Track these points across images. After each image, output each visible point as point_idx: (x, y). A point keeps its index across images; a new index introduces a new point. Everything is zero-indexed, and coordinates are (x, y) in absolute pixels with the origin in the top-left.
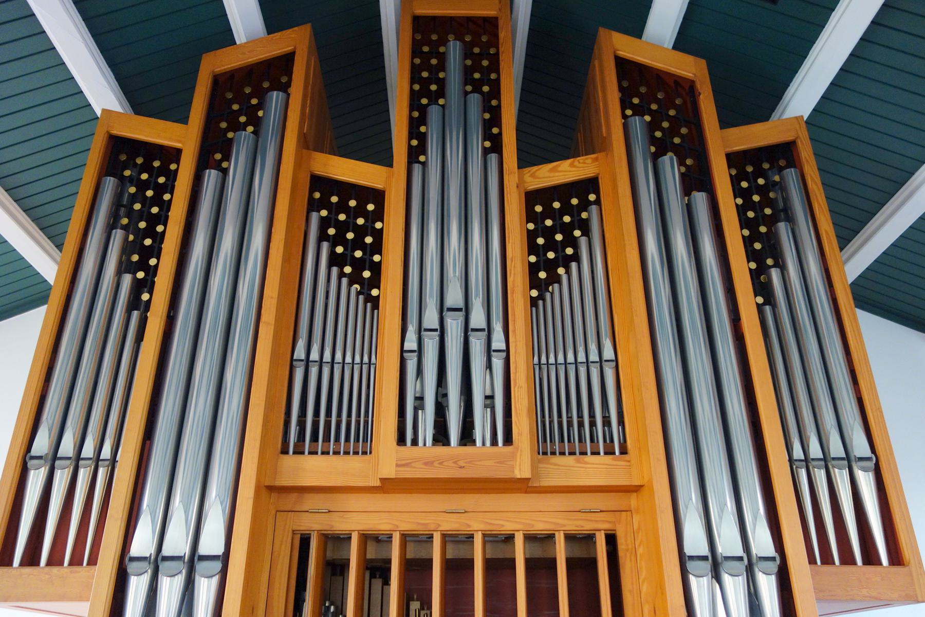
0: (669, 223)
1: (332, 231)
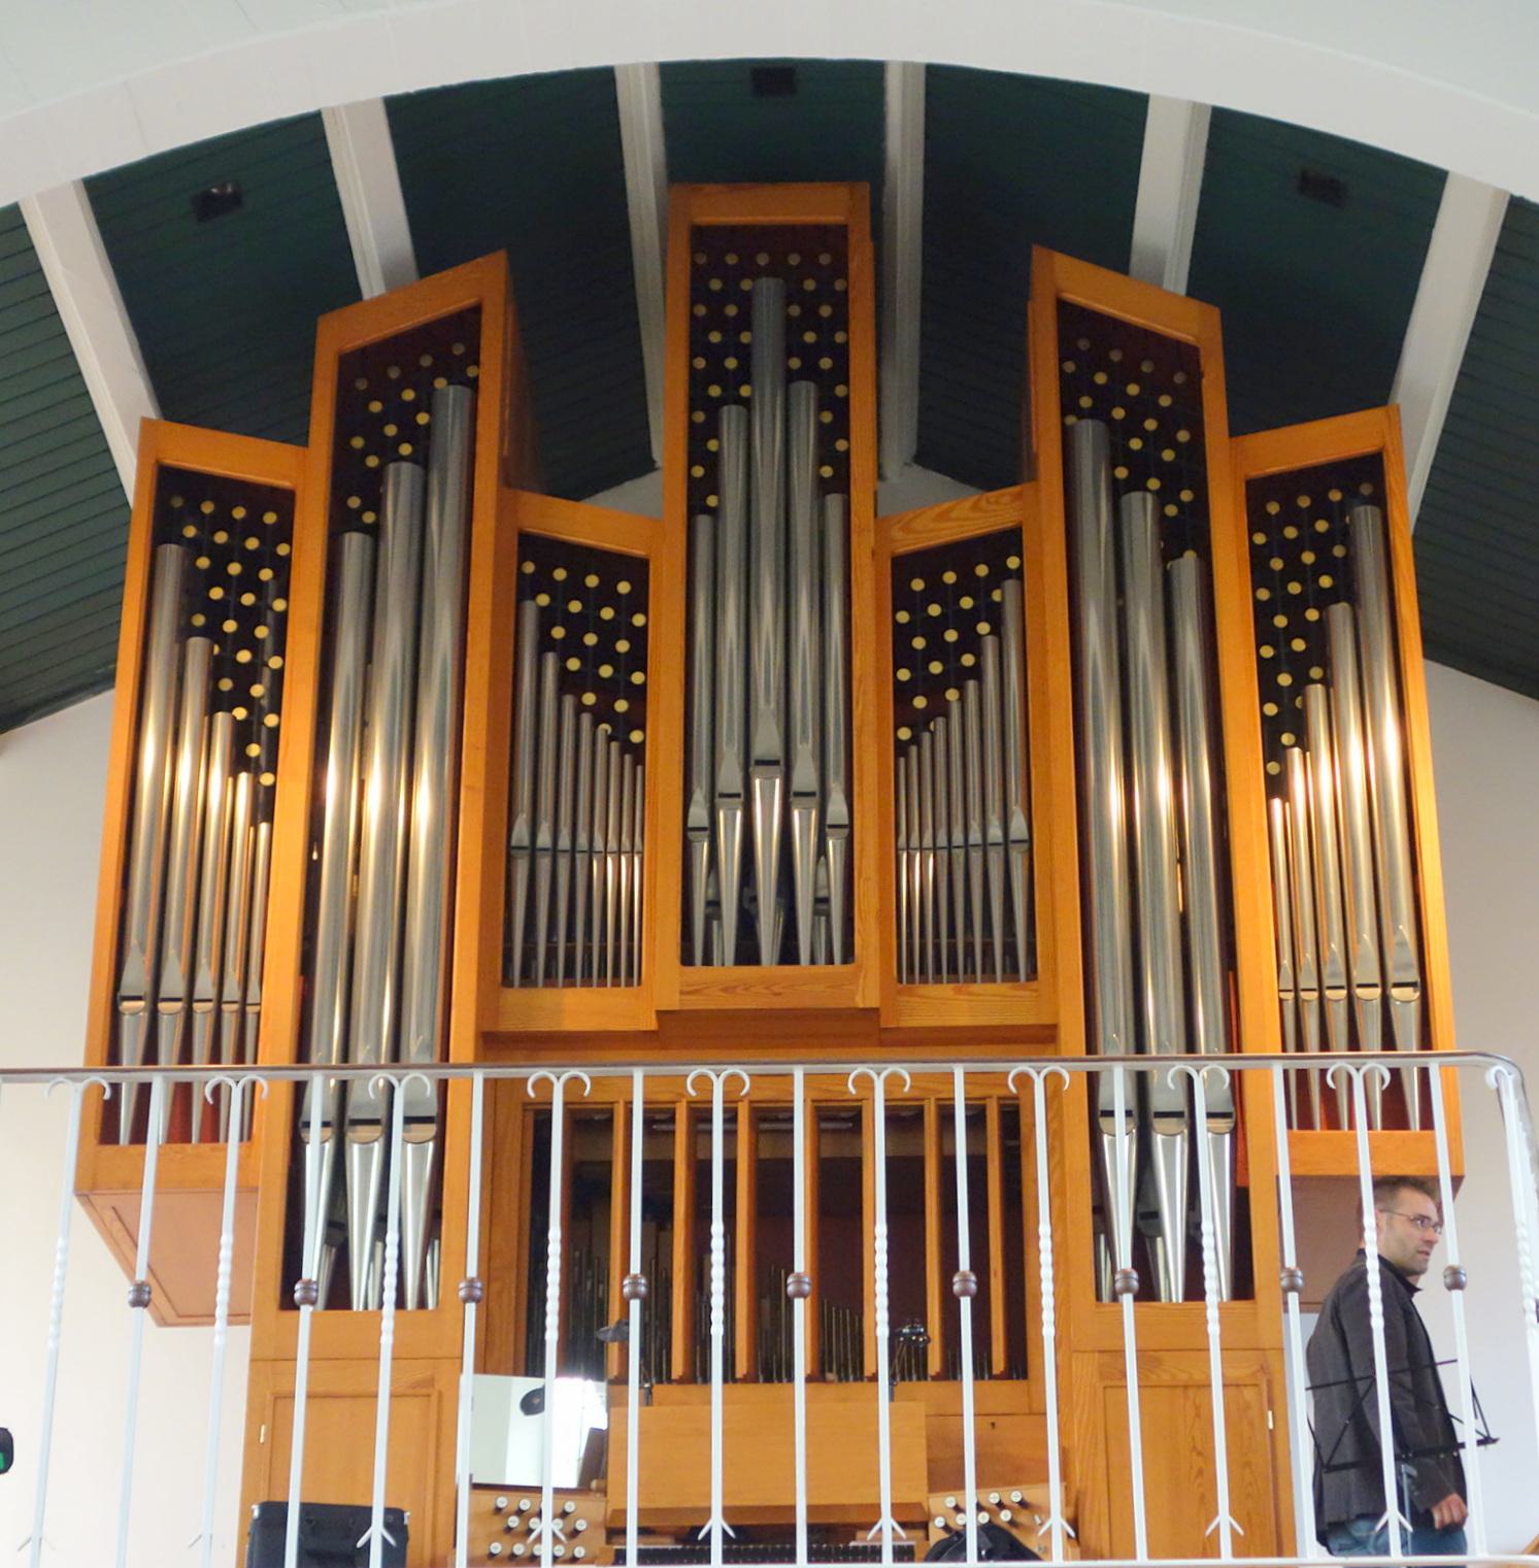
0: (1177, 601)
1: (558, 632)
